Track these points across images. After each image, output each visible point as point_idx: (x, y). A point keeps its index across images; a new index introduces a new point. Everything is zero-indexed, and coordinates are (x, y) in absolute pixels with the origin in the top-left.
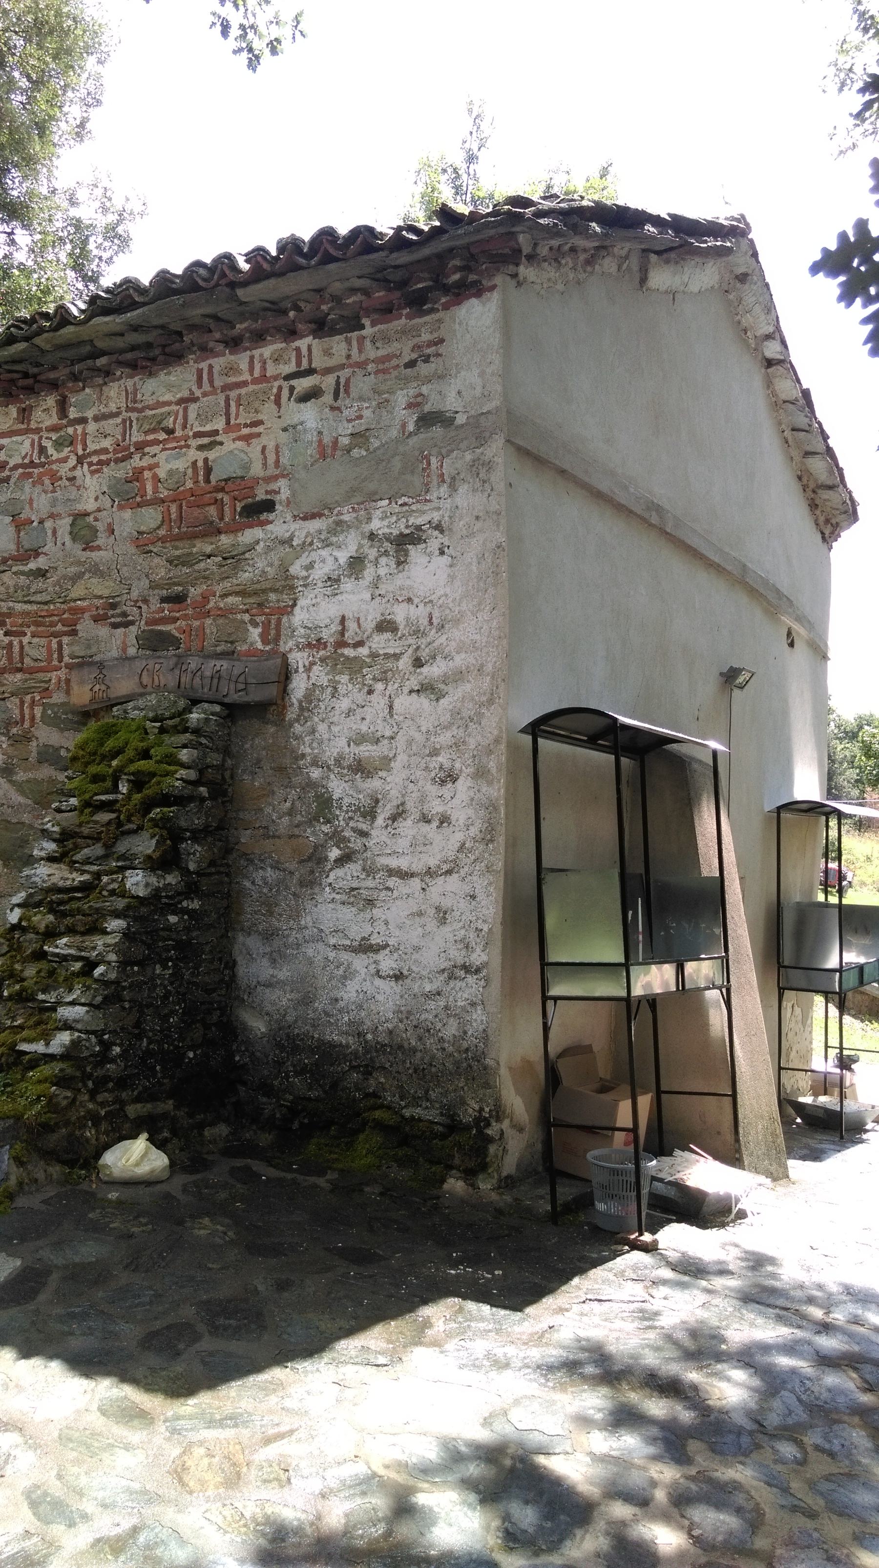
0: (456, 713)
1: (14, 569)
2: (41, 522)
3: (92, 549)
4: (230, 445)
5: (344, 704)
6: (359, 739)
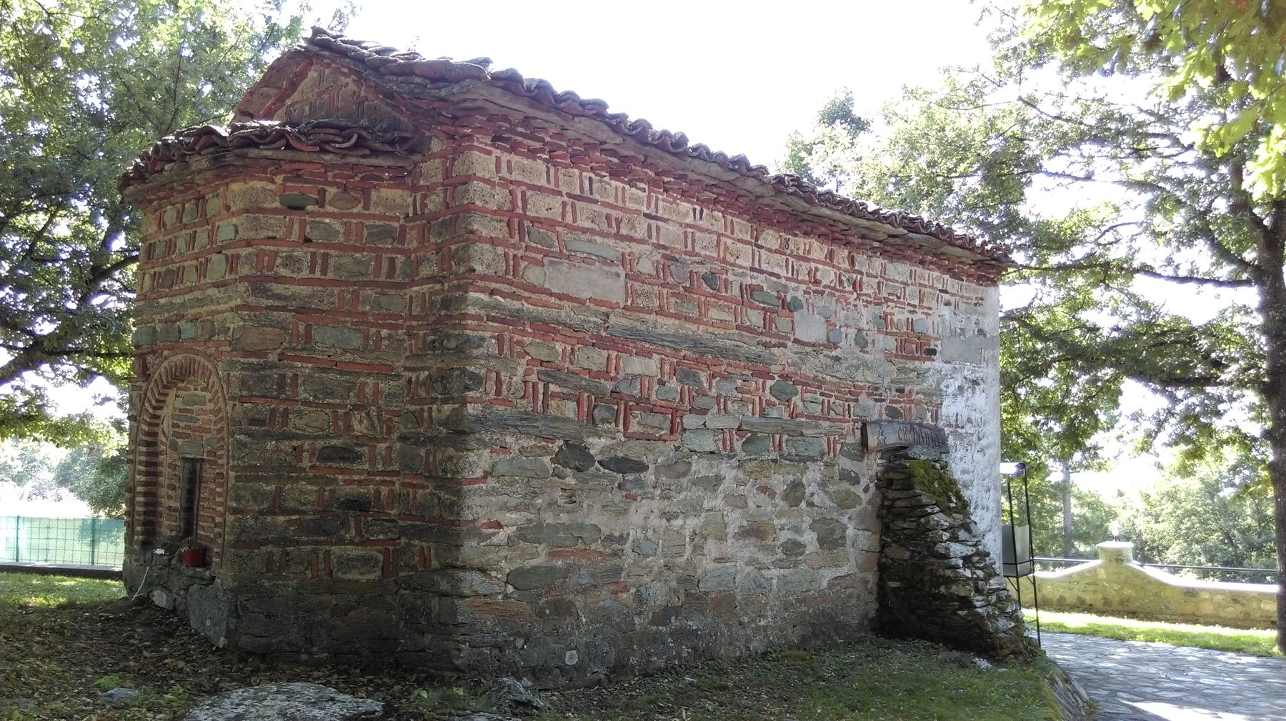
5: (959, 455)
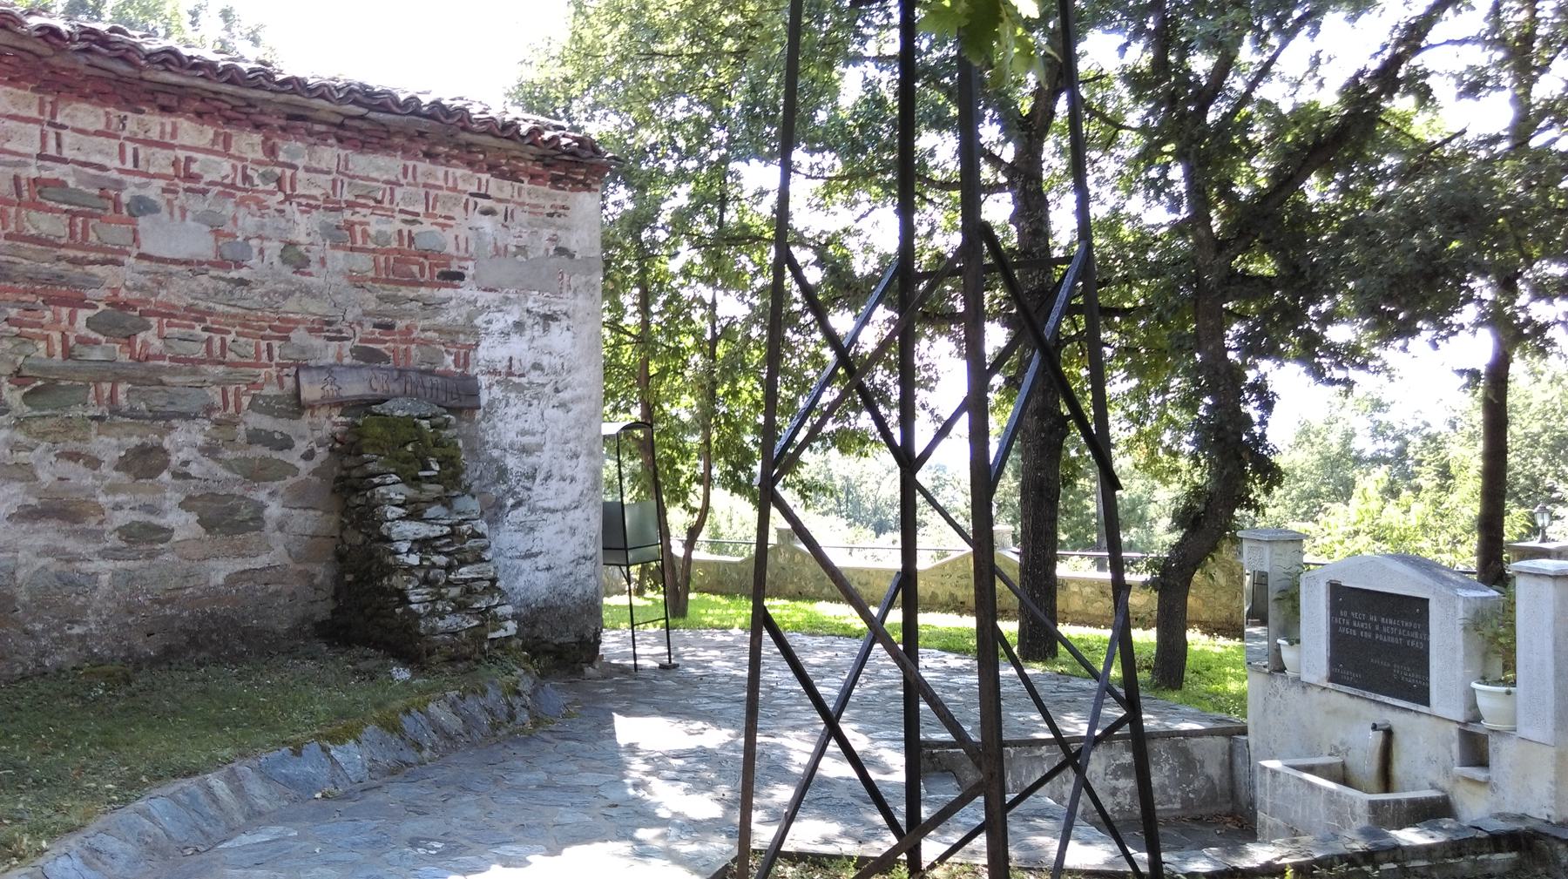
0: (577, 420)
2: (247, 239)
3: (303, 274)
4: (427, 226)
5: (513, 411)
6: (523, 433)
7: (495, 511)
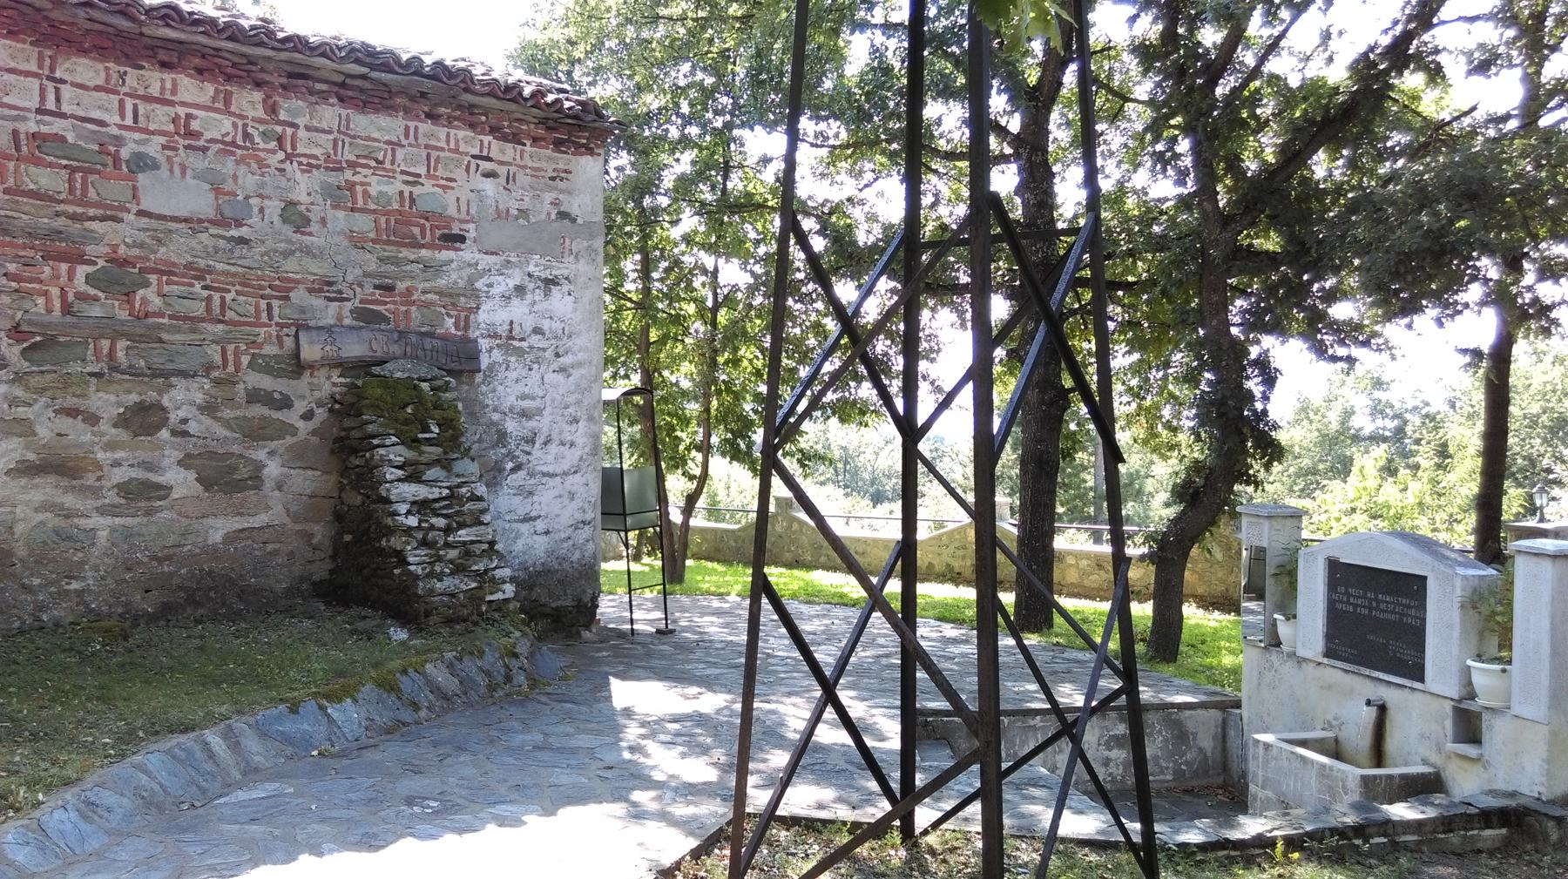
1: (211, 231)
2: (247, 198)
3: (303, 233)
4: (428, 187)
5: (513, 375)
6: (523, 397)
7: (493, 476)
